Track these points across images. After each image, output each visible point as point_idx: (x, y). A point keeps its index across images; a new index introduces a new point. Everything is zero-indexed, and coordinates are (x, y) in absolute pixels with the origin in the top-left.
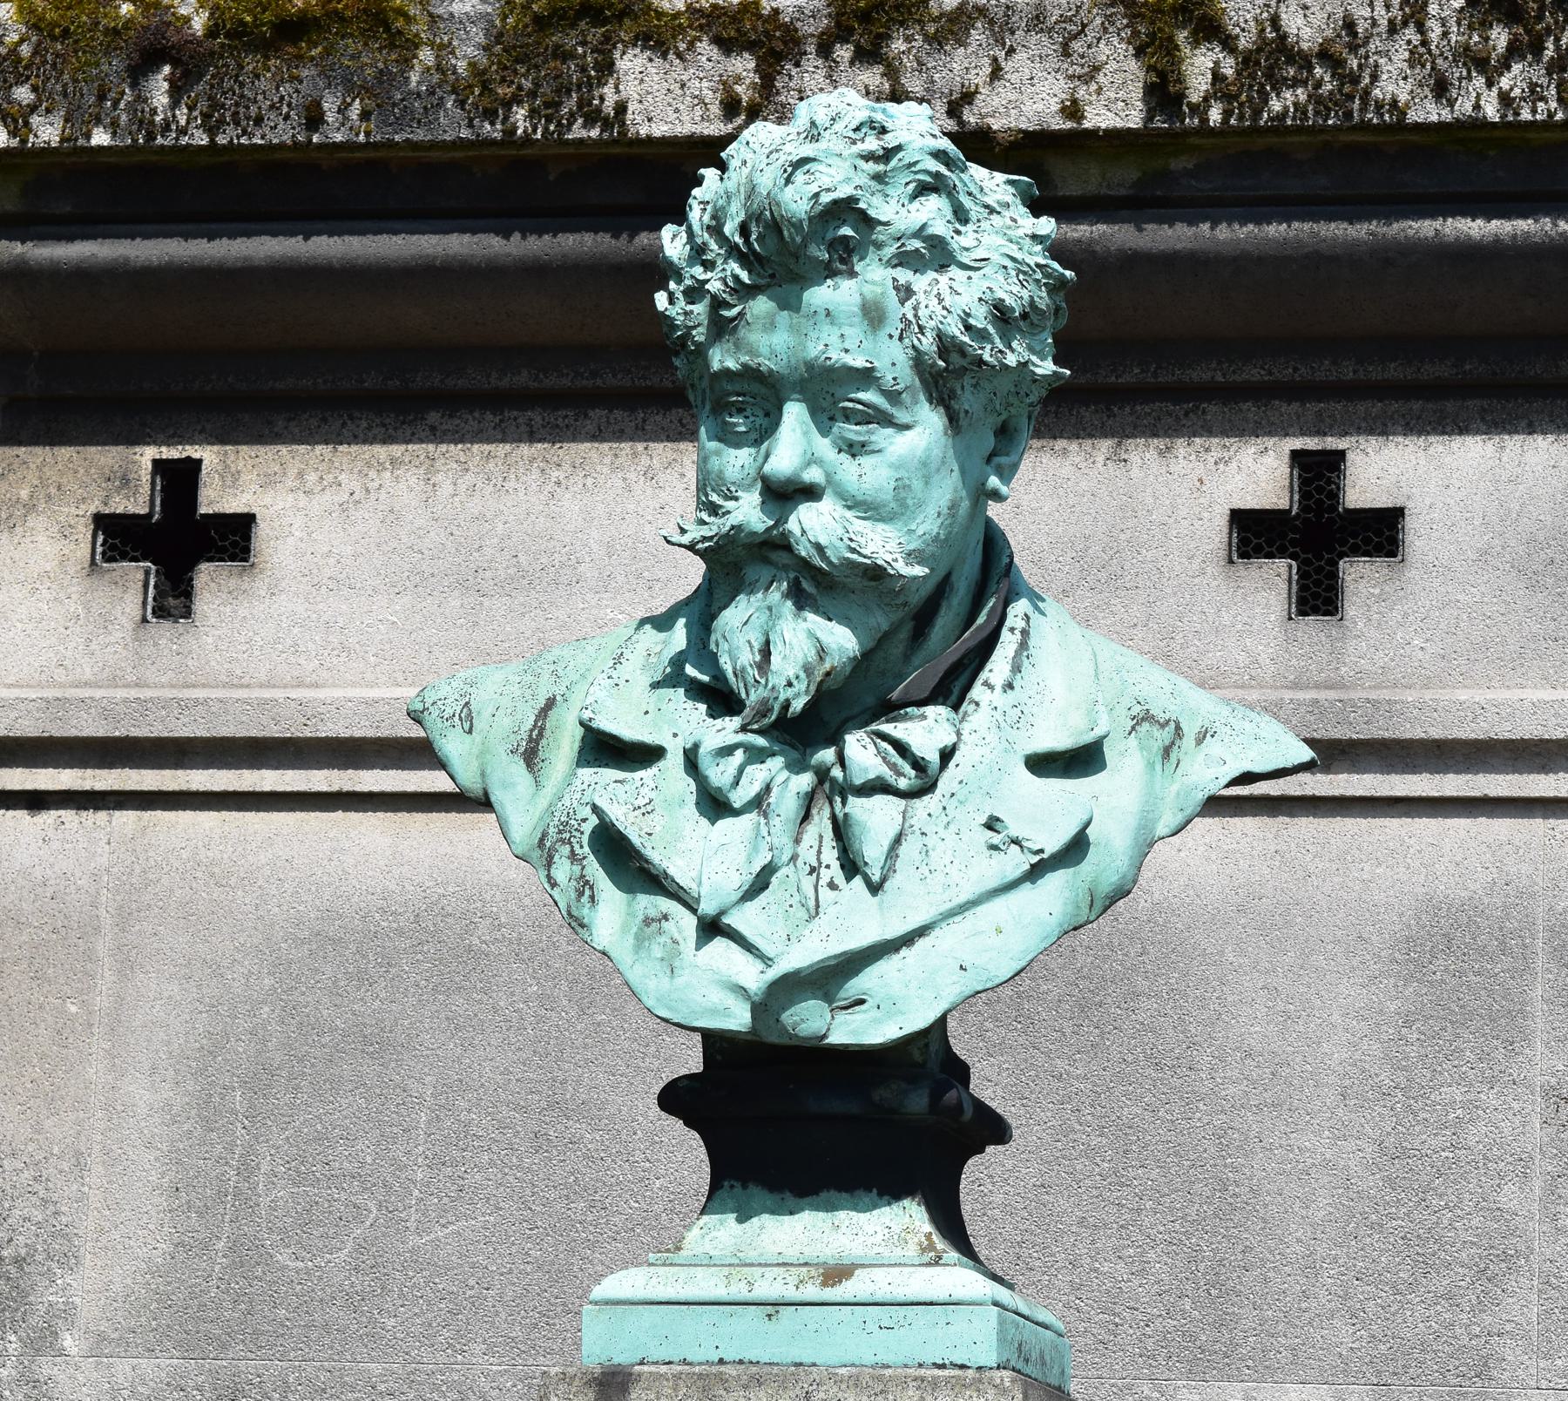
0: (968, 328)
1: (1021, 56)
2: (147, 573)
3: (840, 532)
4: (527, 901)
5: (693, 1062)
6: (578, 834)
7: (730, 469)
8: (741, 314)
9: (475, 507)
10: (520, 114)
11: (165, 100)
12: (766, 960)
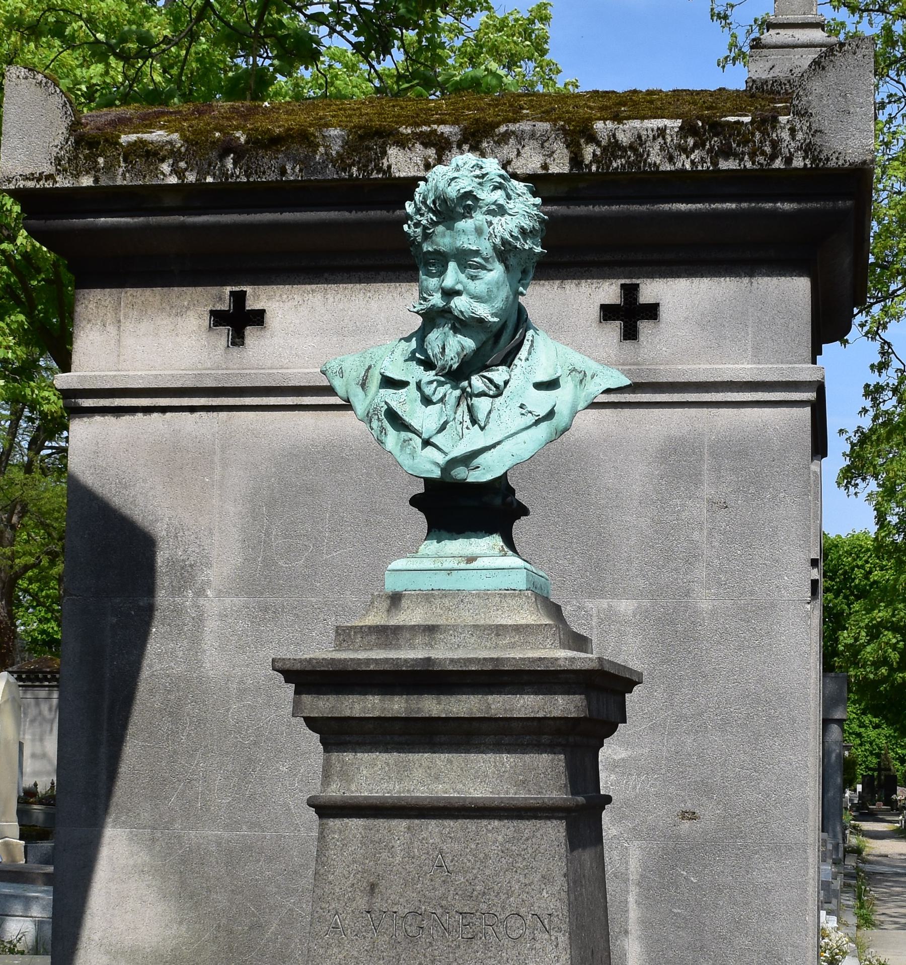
0: (512, 236)
2: (229, 330)
3: (469, 306)
4: (362, 441)
5: (421, 489)
8: (433, 232)
9: (341, 306)
10: (354, 169)
11: (232, 166)
12: (446, 454)
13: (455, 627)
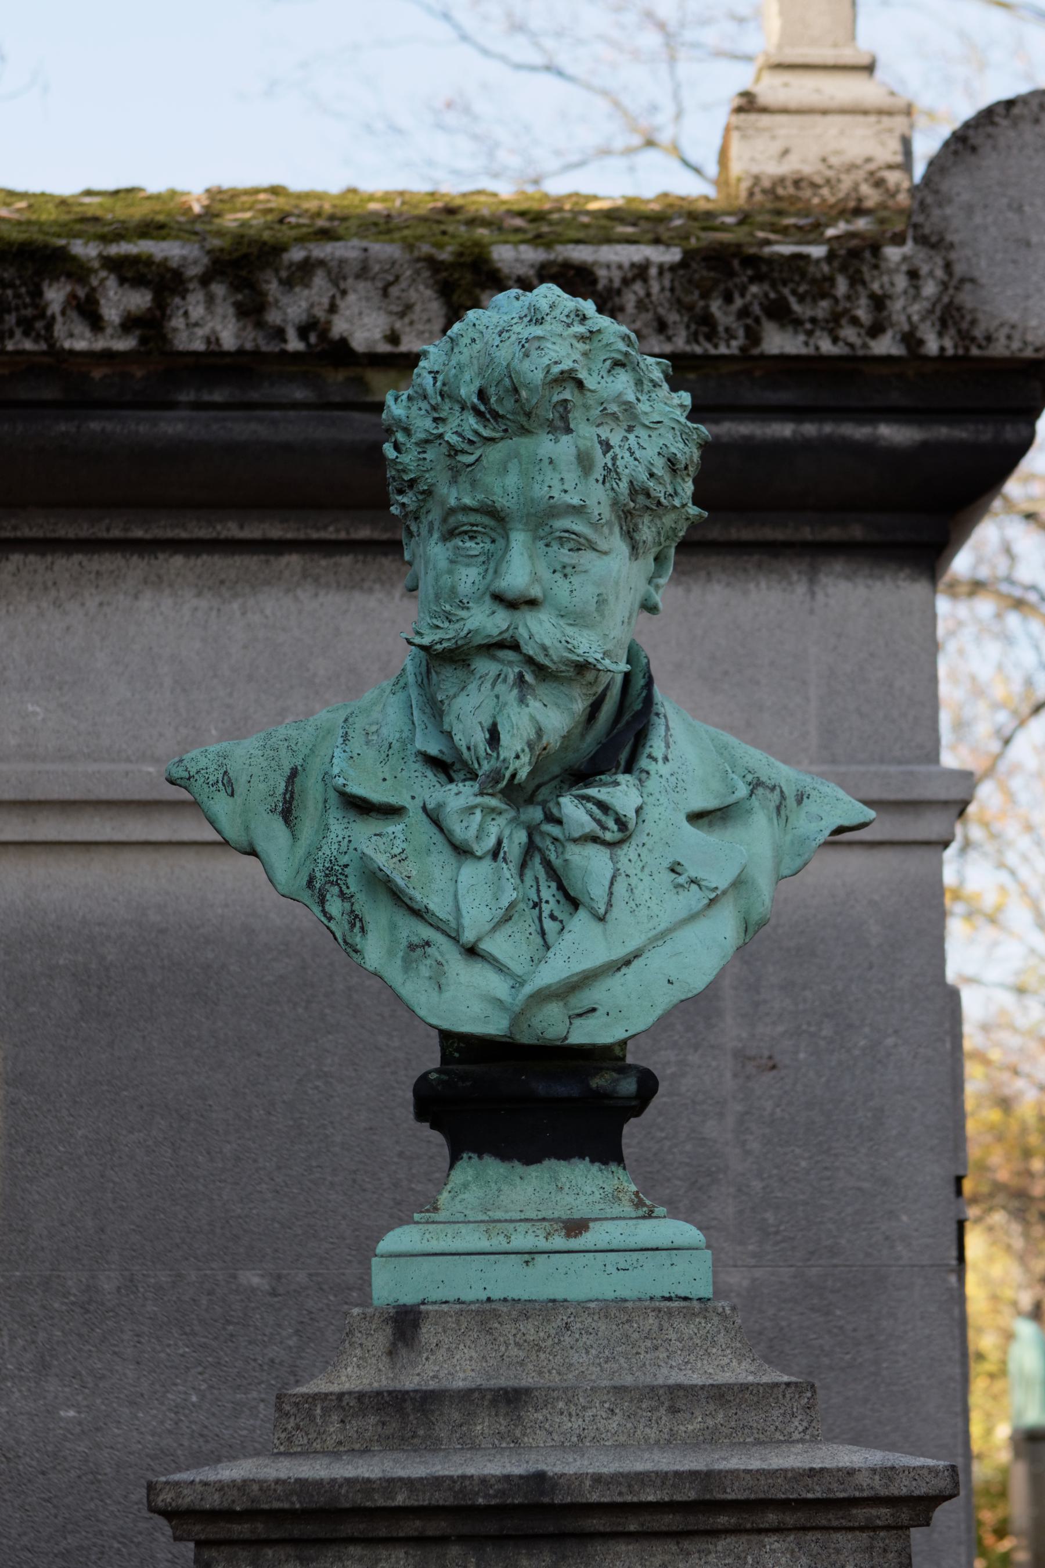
0: (652, 475)
1: (352, 297)
3: (559, 636)
6: (343, 877)
7: (463, 585)
13: (569, 1393)
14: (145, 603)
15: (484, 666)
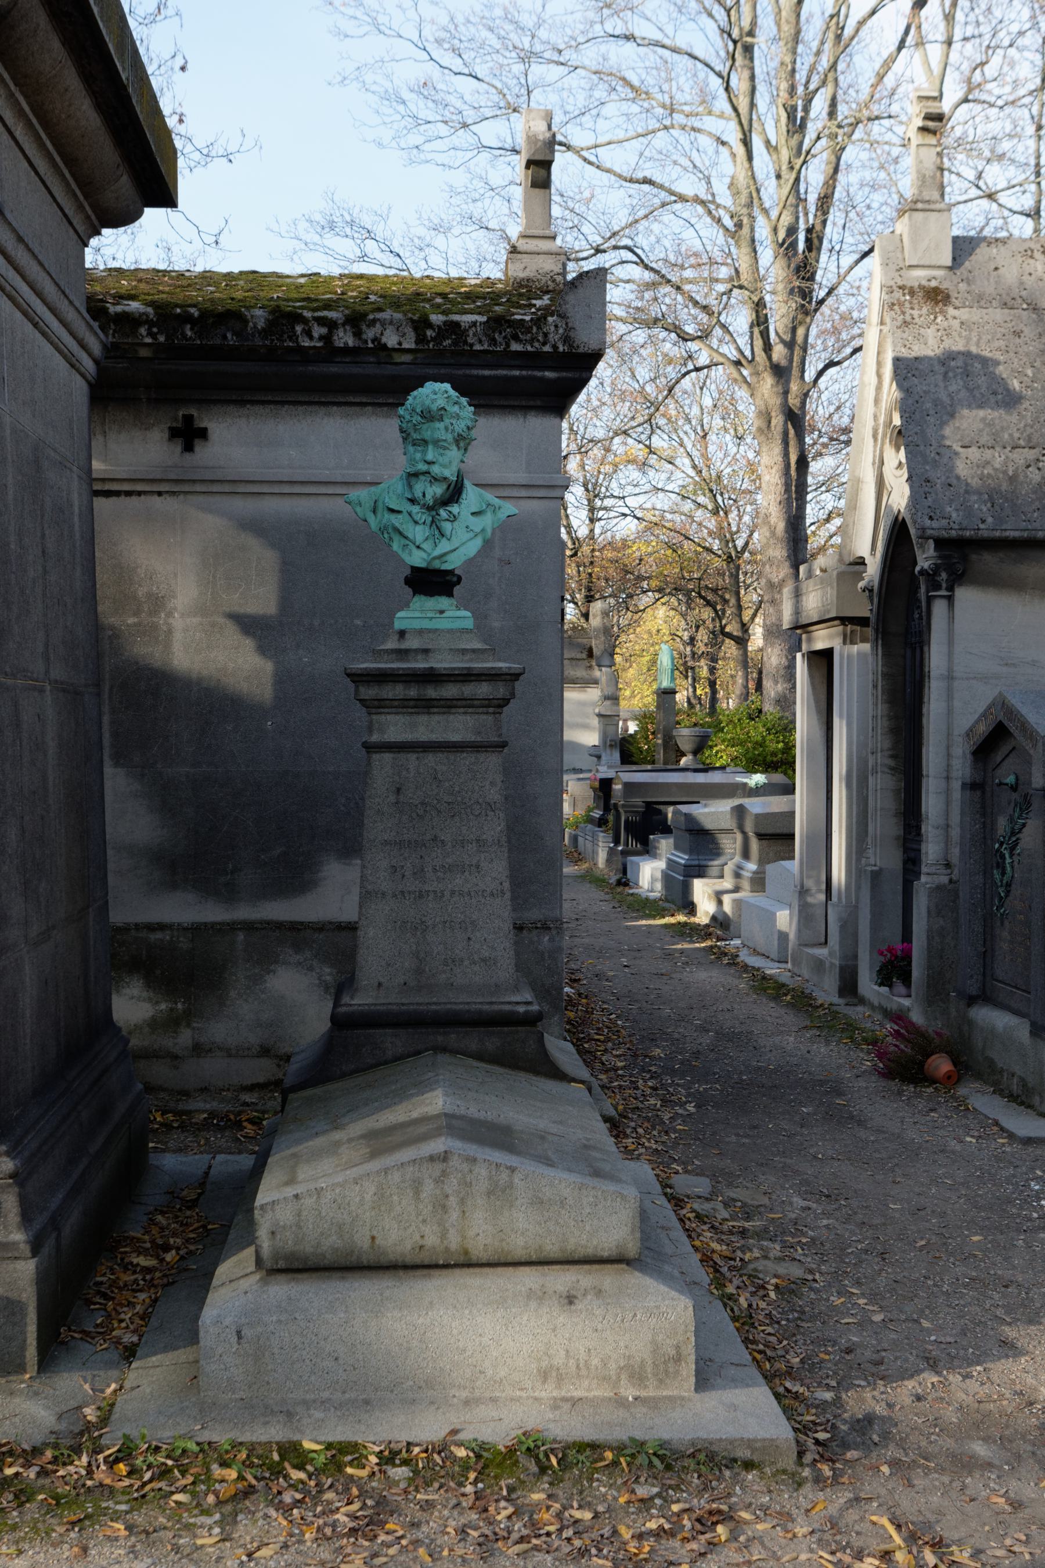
14: (325, 421)
15: (422, 477)
